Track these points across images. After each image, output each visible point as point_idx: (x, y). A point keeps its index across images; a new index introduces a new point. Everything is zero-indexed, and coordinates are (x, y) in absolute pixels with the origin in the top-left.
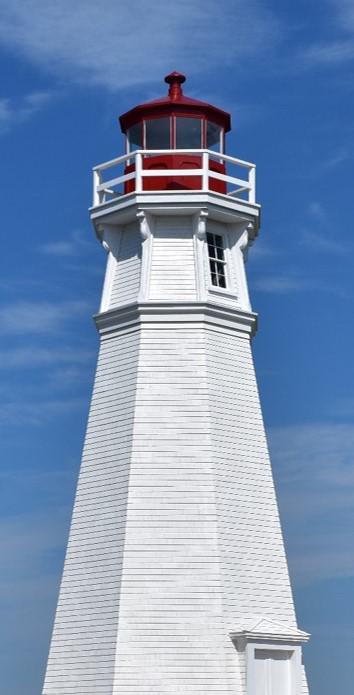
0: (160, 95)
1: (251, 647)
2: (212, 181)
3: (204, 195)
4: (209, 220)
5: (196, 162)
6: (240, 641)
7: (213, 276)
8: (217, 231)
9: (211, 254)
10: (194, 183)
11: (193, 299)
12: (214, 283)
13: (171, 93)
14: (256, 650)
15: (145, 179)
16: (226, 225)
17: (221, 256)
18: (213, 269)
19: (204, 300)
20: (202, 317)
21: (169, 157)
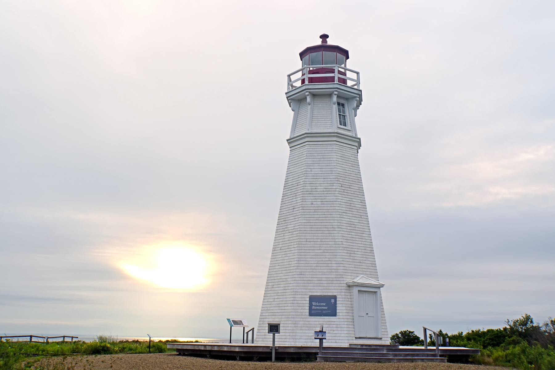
0: (319, 42)
1: (355, 290)
2: (339, 78)
3: (336, 84)
4: (338, 97)
5: (333, 71)
6: (325, 77)
7: (340, 121)
8: (342, 101)
9: (339, 111)
10: (332, 79)
11: (330, 131)
12: (341, 124)
13: (322, 42)
14: (359, 291)
15: (309, 78)
16: (347, 99)
17: (344, 112)
18: (340, 118)
19: (336, 131)
20: (335, 139)
21: (323, 68)
